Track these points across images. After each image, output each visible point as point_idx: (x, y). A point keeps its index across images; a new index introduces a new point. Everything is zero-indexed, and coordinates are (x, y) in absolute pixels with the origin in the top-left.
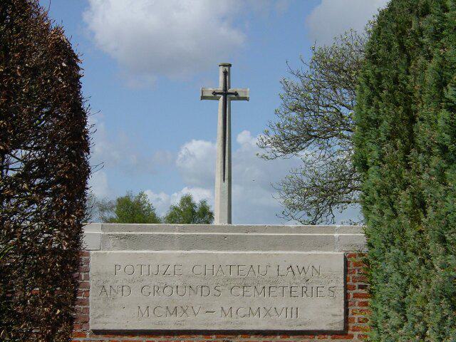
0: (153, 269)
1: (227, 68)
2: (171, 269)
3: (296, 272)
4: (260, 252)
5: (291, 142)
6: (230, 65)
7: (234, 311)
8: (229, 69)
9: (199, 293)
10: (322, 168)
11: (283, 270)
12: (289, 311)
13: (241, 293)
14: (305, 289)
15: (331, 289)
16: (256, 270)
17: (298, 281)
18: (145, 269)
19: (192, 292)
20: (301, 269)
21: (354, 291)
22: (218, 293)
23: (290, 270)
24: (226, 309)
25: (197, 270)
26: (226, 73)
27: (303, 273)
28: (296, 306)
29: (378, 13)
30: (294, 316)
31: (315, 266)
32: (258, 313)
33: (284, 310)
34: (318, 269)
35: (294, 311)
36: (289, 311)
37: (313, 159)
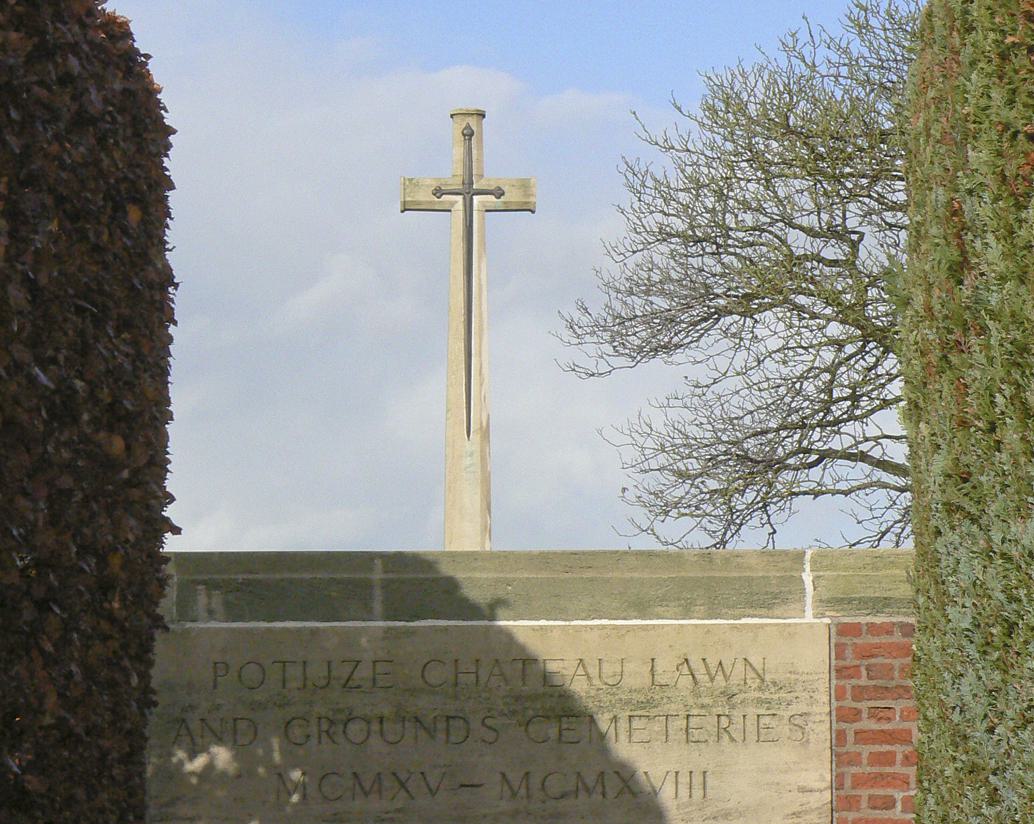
0: (317, 672)
1: (473, 122)
2: (364, 673)
3: (702, 677)
4: (605, 622)
5: (653, 324)
6: (482, 115)
7: (536, 781)
8: (480, 126)
9: (441, 736)
10: (741, 400)
11: (666, 666)
12: (684, 779)
13: (553, 732)
14: (724, 721)
15: (798, 721)
16: (593, 671)
17: (707, 701)
18: (294, 672)
19: (422, 734)
20: (713, 663)
21: (857, 726)
22: (490, 736)
23: (685, 670)
24: (515, 777)
25: (435, 675)
26: (468, 134)
27: (720, 678)
28: (691, 767)
29: (112, 10)
30: (698, 793)
31: (752, 660)
32: (599, 789)
33: (671, 778)
34: (759, 668)
35: (697, 780)
36: (684, 779)
37: (738, 370)
